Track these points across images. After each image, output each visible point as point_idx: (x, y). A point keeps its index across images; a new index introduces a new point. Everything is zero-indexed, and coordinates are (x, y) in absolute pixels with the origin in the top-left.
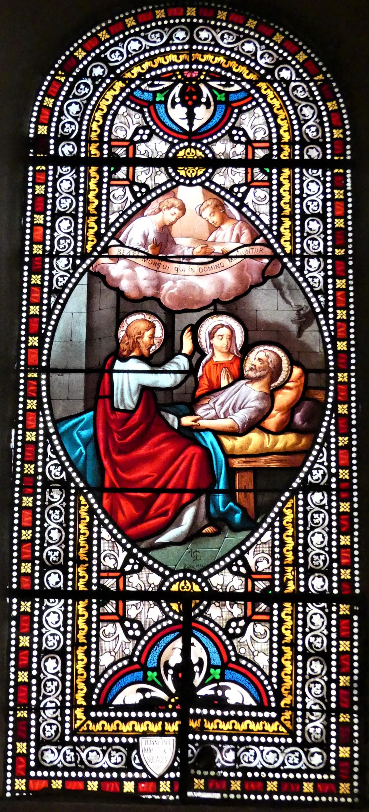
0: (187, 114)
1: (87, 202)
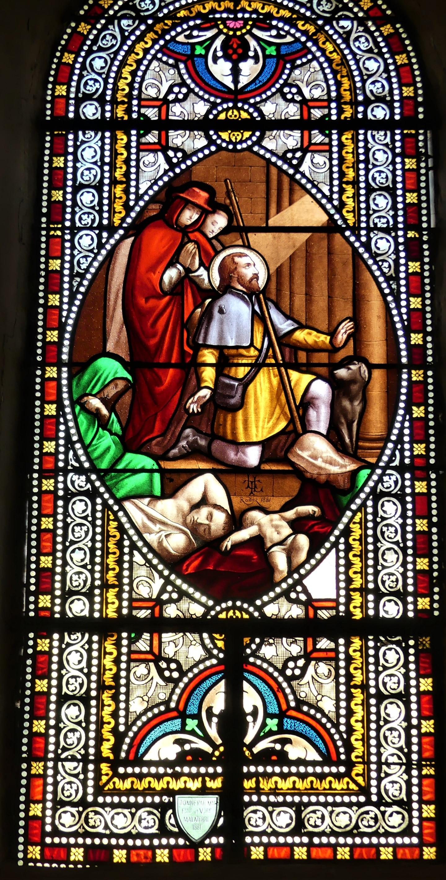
0: (231, 69)
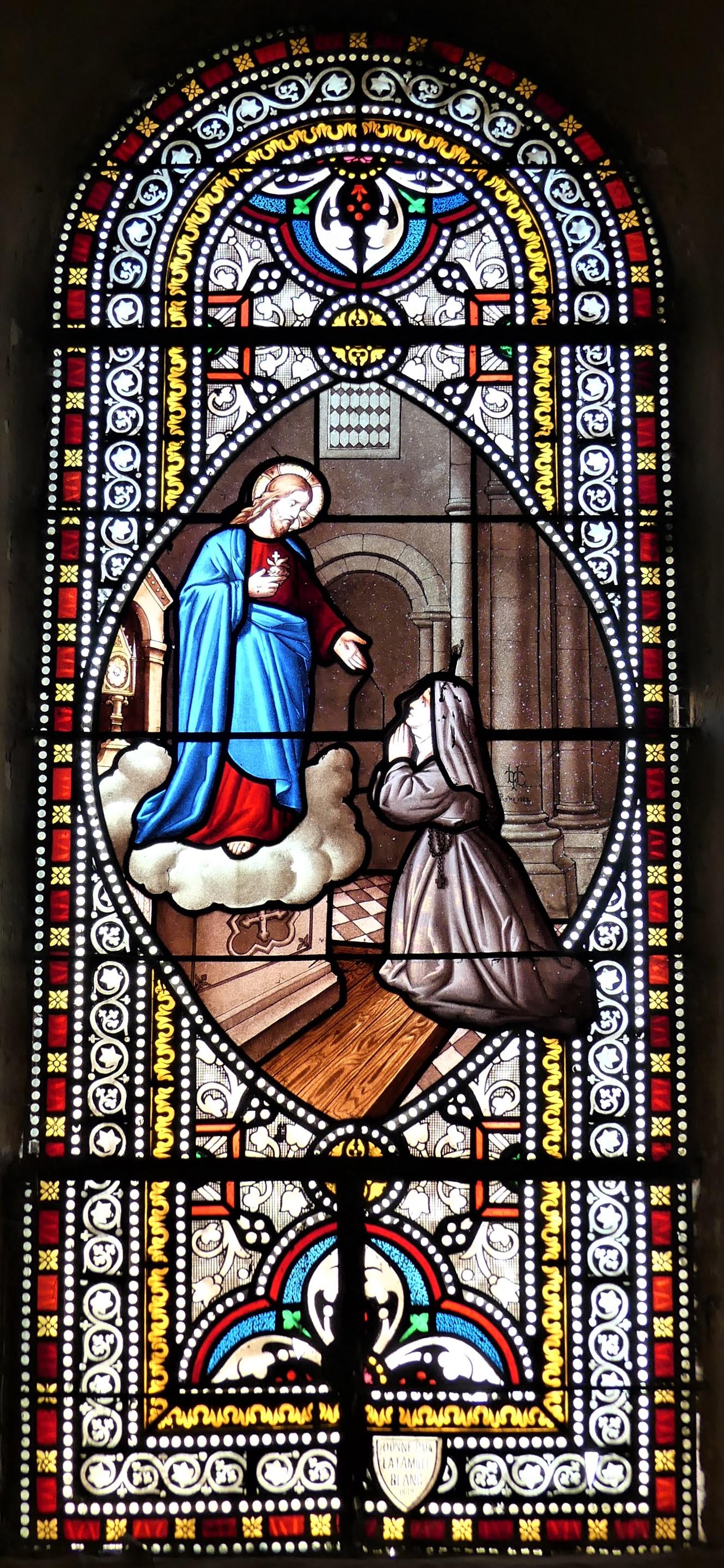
0: (352, 240)
1: (164, 414)
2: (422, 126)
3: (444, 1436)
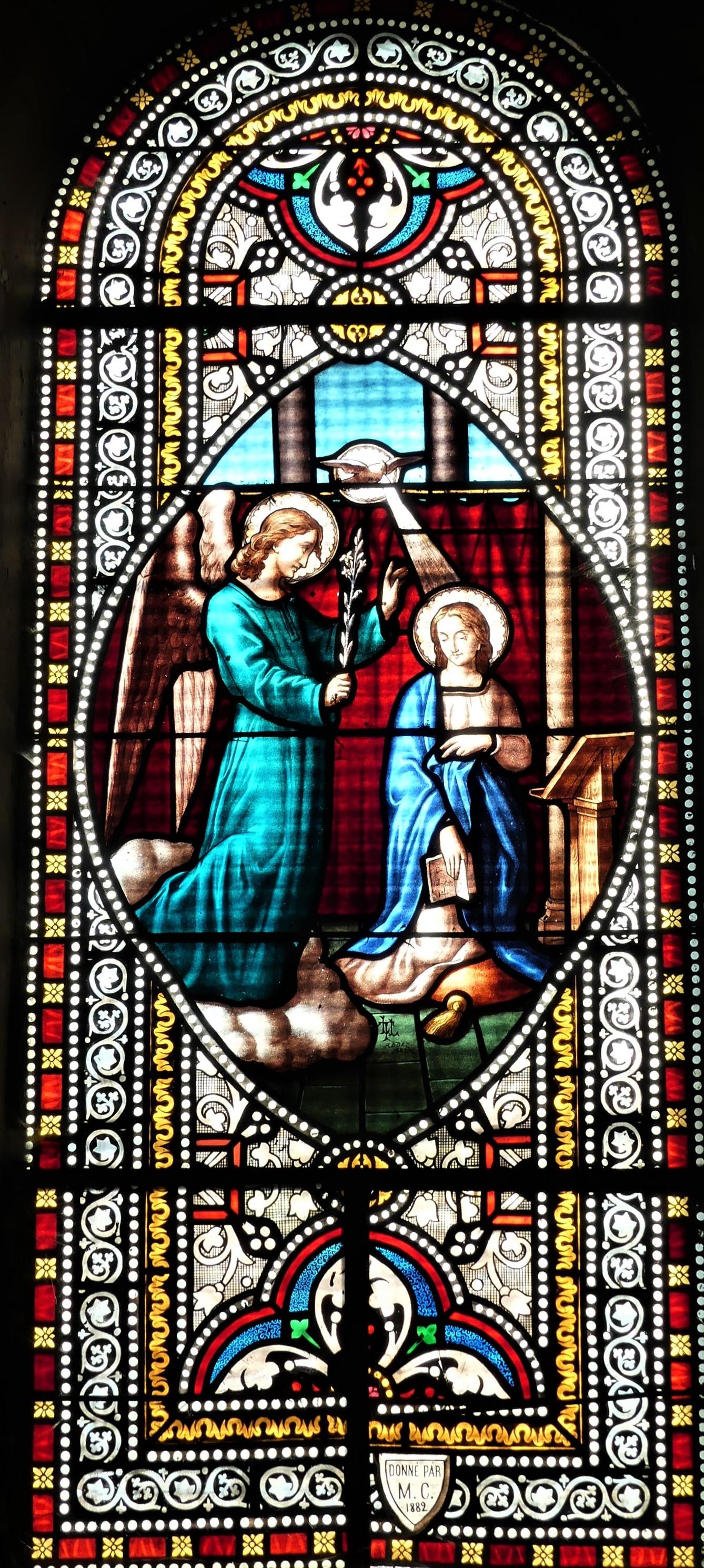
2: (429, 95)
3: (452, 1454)
